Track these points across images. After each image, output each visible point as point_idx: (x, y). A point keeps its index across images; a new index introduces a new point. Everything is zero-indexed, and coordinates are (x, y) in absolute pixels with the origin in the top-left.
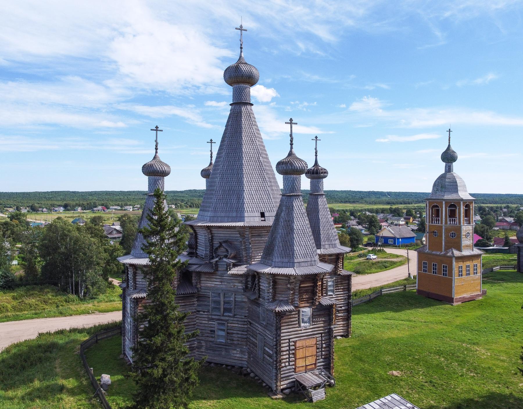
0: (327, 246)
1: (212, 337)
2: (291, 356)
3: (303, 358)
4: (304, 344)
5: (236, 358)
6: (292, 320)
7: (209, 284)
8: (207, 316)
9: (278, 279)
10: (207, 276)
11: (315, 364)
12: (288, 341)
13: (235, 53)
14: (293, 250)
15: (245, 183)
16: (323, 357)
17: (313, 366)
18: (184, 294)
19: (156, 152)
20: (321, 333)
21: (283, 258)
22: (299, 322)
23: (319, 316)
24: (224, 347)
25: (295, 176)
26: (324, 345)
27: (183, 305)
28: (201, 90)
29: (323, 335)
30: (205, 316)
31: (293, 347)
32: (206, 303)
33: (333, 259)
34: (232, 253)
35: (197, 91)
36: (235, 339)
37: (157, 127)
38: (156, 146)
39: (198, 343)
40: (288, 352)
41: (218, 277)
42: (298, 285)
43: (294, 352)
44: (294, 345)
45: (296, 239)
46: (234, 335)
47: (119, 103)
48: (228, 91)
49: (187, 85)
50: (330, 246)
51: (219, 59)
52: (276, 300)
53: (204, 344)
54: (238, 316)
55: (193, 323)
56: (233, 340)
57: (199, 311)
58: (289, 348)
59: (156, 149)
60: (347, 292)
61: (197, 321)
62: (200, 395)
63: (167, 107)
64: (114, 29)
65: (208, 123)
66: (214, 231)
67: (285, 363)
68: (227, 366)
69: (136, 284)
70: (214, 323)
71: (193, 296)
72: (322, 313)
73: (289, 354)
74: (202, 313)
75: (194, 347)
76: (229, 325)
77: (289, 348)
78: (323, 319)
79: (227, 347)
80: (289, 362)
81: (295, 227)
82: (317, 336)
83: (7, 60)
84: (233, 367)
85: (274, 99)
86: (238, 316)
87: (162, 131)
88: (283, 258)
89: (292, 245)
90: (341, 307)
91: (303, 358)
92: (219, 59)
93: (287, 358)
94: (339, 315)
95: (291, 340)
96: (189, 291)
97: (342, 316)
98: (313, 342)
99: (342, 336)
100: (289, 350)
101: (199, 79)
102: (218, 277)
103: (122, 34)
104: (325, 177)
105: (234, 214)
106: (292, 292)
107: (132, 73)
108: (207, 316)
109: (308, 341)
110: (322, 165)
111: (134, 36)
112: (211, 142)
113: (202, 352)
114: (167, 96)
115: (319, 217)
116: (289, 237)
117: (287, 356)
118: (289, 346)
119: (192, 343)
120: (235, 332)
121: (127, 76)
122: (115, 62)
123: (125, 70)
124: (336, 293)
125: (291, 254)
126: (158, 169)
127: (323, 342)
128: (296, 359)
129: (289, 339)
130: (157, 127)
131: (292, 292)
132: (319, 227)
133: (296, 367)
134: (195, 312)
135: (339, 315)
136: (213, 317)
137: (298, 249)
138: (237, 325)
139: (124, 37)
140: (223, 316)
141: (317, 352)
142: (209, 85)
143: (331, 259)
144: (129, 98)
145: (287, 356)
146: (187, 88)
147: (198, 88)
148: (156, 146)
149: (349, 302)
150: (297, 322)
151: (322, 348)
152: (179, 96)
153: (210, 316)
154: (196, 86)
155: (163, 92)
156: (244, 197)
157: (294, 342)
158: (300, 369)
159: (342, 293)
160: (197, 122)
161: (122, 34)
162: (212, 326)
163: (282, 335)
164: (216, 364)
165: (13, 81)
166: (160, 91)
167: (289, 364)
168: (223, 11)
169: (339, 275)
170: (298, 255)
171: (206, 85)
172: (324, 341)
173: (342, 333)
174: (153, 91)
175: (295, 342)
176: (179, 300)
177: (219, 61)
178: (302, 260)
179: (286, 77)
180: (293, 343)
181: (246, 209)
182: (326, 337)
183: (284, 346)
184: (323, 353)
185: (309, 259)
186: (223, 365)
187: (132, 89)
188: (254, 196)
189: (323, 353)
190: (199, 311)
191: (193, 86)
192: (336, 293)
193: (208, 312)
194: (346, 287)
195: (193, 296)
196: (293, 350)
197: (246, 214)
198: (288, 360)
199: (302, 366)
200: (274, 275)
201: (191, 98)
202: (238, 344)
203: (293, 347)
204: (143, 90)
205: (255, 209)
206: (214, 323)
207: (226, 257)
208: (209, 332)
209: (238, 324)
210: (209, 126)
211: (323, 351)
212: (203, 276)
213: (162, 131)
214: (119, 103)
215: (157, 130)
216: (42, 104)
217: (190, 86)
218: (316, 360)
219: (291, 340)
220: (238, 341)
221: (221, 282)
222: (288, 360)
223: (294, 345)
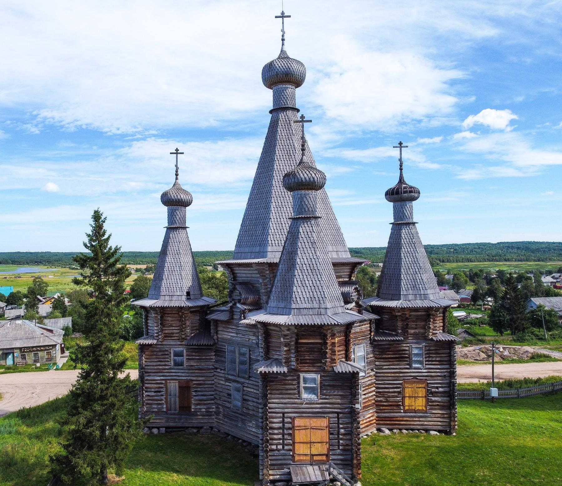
0: (411, 297)
1: (228, 402)
2: (286, 437)
3: (306, 443)
4: (308, 424)
5: (252, 433)
6: (287, 387)
7: (227, 334)
8: (223, 375)
9: (271, 330)
10: (224, 326)
11: (327, 455)
12: (281, 415)
13: (467, 73)
14: (291, 292)
15: (273, 209)
16: (341, 448)
17: (324, 458)
18: (198, 345)
19: (177, 179)
20: (338, 413)
21: (279, 302)
22: (299, 392)
23: (333, 387)
24: (240, 416)
25: (303, 192)
26: (342, 431)
27: (198, 359)
28: (422, 124)
29: (341, 415)
30: (221, 375)
31: (290, 425)
32: (223, 359)
33: (421, 315)
34: (251, 298)
35: (418, 125)
36: (250, 408)
37: (177, 150)
38: (177, 171)
39: (217, 408)
40: (281, 431)
41: (233, 327)
42: (294, 339)
43: (291, 432)
44: (290, 423)
45: (297, 276)
46: (250, 403)
47: (326, 149)
48: (266, 98)
49: (405, 120)
50: (416, 297)
51: (445, 83)
52: (269, 358)
53: (221, 410)
54: (253, 379)
55: (210, 382)
56: (248, 409)
57: (217, 368)
58: (284, 425)
59: (177, 175)
60: (447, 366)
61: (215, 380)
62: (176, 467)
63: (381, 149)
64: (319, 71)
65: (433, 162)
66: (237, 270)
67: (277, 445)
68: (244, 441)
69: (148, 329)
70: (230, 384)
71: (210, 349)
72: (338, 383)
73: (283, 435)
74: (219, 370)
75: (212, 412)
76: (245, 388)
77: (284, 425)
78: (340, 393)
79: (243, 418)
80: (283, 445)
81: (298, 260)
82: (330, 415)
83: (217, 121)
84: (250, 444)
85: (512, 122)
86: (253, 379)
87: (183, 153)
88: (279, 302)
89: (291, 285)
90: (437, 388)
91: (306, 443)
92: (445, 83)
93: (280, 439)
94: (433, 399)
95: (286, 415)
96: (204, 342)
97: (439, 402)
98: (324, 422)
99: (439, 431)
100: (283, 428)
101: (420, 111)
102: (233, 327)
103: (327, 75)
104: (415, 199)
105: (257, 249)
106: (285, 349)
107: (339, 116)
108: (223, 375)
109: (315, 420)
110: (410, 181)
111: (341, 74)
112: (177, 153)
113: (220, 419)
114: (381, 136)
115: (400, 256)
116: (290, 274)
117: (280, 436)
118: (283, 422)
119: (209, 406)
120: (250, 398)
121: (334, 119)
122: (321, 106)
123: (331, 113)
124: (428, 366)
125: (289, 296)
126: (173, 197)
127: (341, 426)
128: (294, 443)
129: (284, 413)
130: (177, 150)
131: (285, 349)
132: (400, 269)
133: (294, 453)
134: (212, 369)
135: (433, 399)
136: (230, 377)
137: (299, 291)
138: (252, 390)
139: (329, 77)
140: (238, 376)
141: (330, 439)
142: (435, 117)
143: (417, 316)
144: (338, 144)
145: (280, 436)
146: (404, 124)
147: (420, 121)
148: (177, 171)
149: (451, 382)
150: (296, 391)
151: (338, 434)
152: (396, 134)
153: (227, 376)
154: (416, 120)
155: (377, 132)
156: (269, 226)
157: (290, 418)
158: (302, 458)
159: (439, 367)
160: (420, 162)
161: (327, 75)
162: (229, 388)
163: (269, 405)
164: (234, 437)
165: (222, 140)
166: (372, 132)
167: (283, 447)
168: (449, 23)
169: (432, 339)
170: (298, 299)
171: (429, 117)
172: (342, 424)
173: (439, 428)
174: (364, 132)
175: (293, 419)
176: (192, 352)
177: (445, 86)
178: (305, 306)
179: (546, 90)
180: (289, 420)
181: (270, 242)
182: (347, 420)
183: (276, 422)
184: (341, 442)
185: (316, 306)
186: (239, 439)
187: (340, 132)
188: (284, 225)
189: (341, 442)
190: (217, 368)
191: (413, 120)
192: (428, 366)
193: (225, 370)
194: (446, 359)
195: (210, 349)
196: (290, 429)
197: (270, 249)
198: (281, 441)
199: (306, 455)
200: (265, 325)
201: (411, 135)
202: (254, 415)
203: (290, 425)
204: (353, 132)
205: (276, 242)
206: (230, 384)
207: (239, 301)
208: (226, 395)
209: (253, 389)
210: (435, 166)
211: (342, 439)
212: (220, 325)
213: (183, 153)
214: (326, 149)
215: (177, 153)
216: (249, 160)
217: (409, 121)
218: (329, 450)
219: (286, 415)
220: (254, 410)
221: (237, 334)
222: (281, 441)
223: (290, 423)
